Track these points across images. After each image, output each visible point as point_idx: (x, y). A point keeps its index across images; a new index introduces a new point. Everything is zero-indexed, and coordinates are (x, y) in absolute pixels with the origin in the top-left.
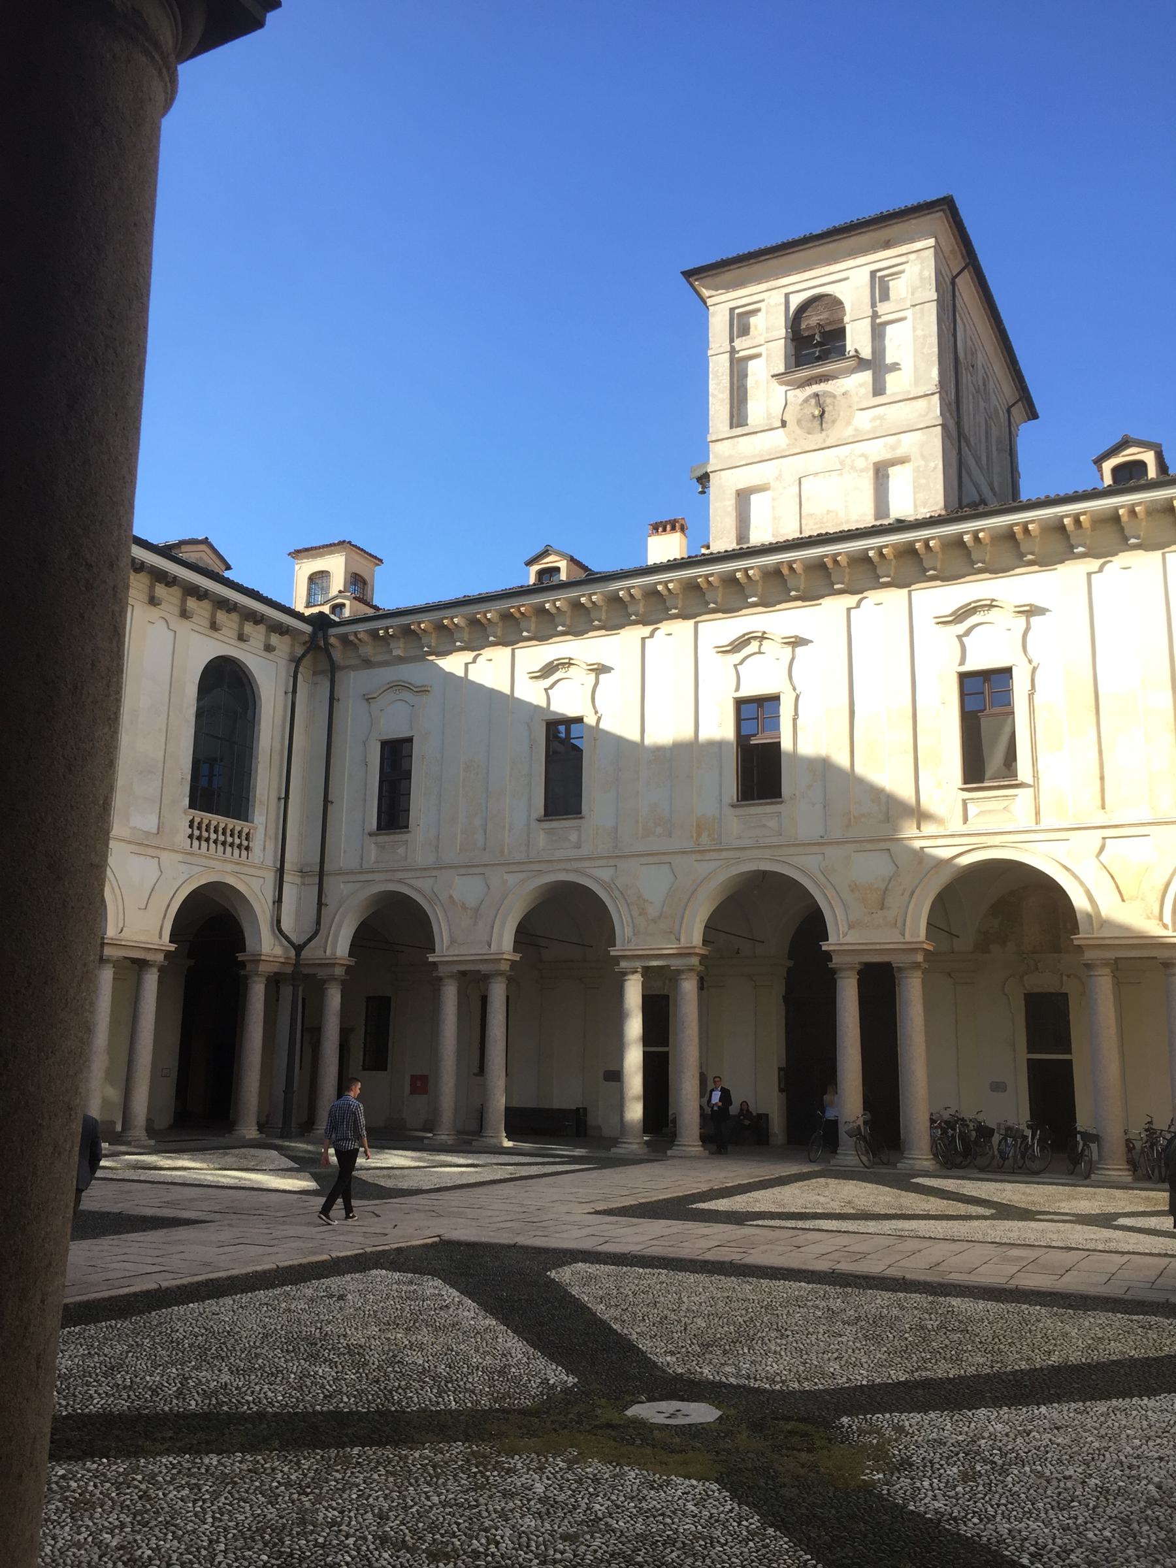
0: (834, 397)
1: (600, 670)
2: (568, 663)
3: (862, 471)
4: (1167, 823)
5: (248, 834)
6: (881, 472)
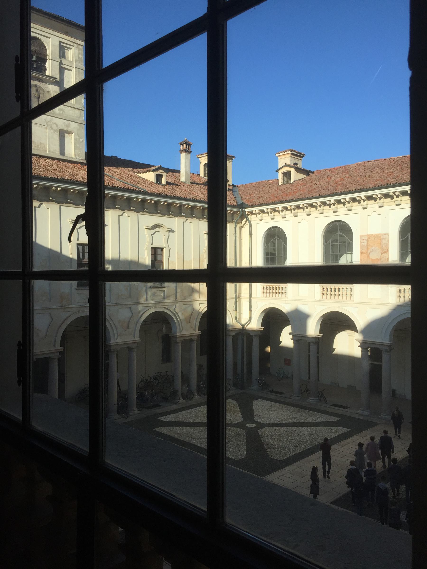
0: (44, 91)
1: (171, 231)
2: (160, 226)
3: (55, 131)
4: (318, 366)
5: (324, 290)
6: (62, 134)
